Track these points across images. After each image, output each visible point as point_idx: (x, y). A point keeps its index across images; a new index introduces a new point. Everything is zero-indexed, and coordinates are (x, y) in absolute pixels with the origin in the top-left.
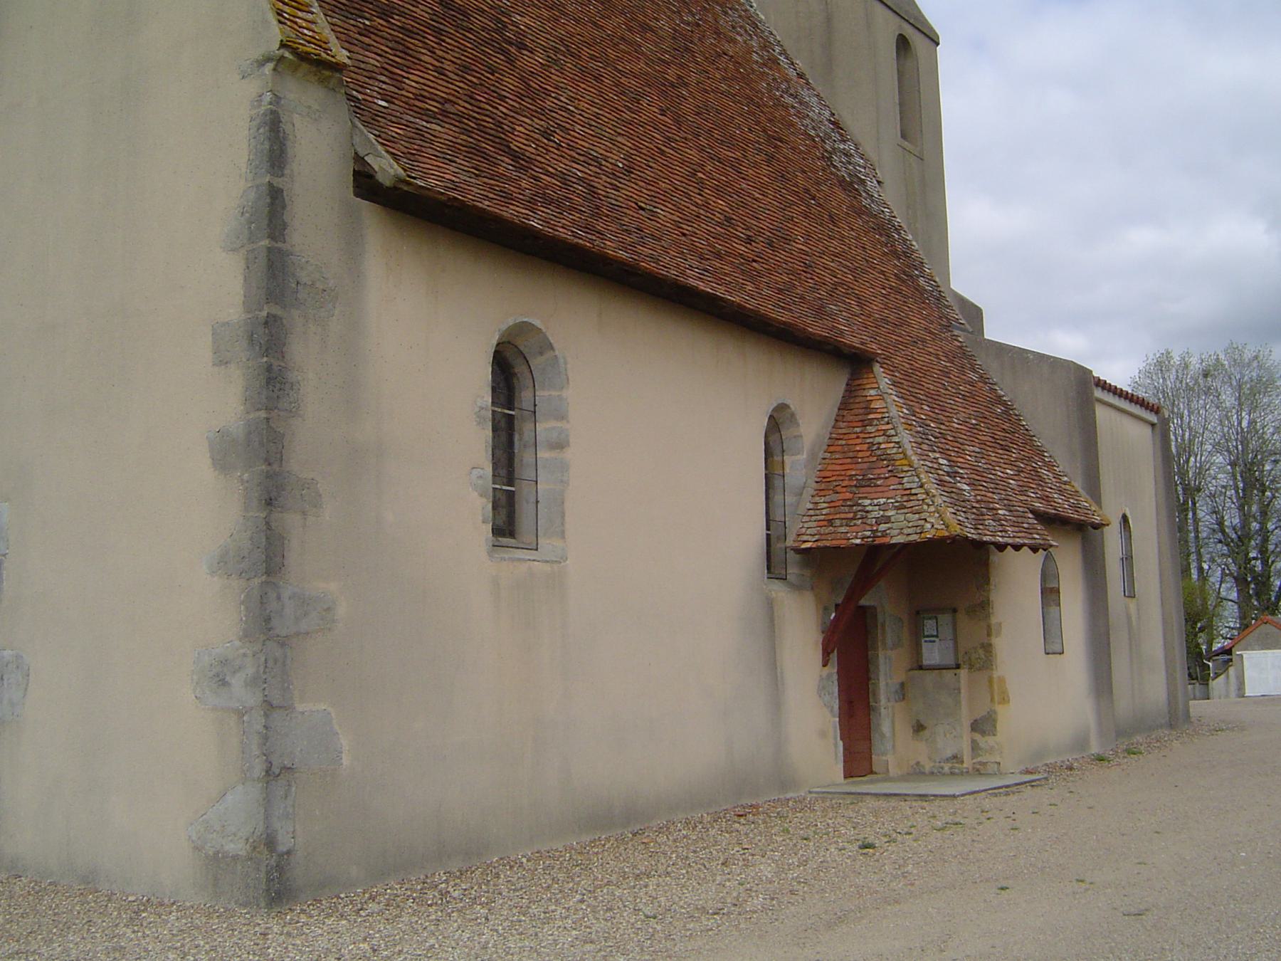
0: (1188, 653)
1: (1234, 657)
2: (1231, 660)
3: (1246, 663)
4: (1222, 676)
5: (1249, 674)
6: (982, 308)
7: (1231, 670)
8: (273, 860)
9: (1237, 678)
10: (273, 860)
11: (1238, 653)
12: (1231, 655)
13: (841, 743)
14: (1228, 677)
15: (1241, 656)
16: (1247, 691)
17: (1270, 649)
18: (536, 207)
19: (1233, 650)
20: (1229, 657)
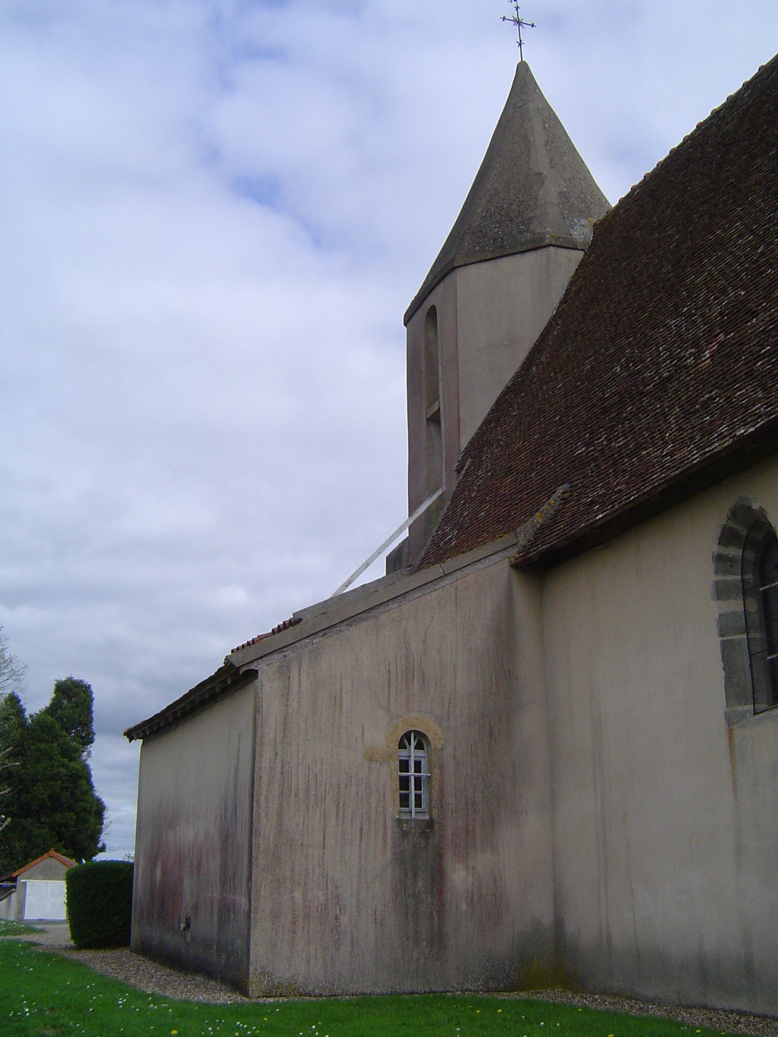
0: (402, 532)
1: (18, 884)
2: (15, 887)
3: (28, 890)
4: (5, 901)
5: (29, 899)
6: (94, 720)
7: (14, 896)
8: (78, 792)
9: (19, 902)
10: (78, 792)
11: (22, 881)
12: (16, 882)
13: (406, 534)
14: (9, 902)
15: (25, 884)
16: (26, 915)
17: (52, 879)
18: (682, 412)
19: (18, 878)
20: (12, 884)
